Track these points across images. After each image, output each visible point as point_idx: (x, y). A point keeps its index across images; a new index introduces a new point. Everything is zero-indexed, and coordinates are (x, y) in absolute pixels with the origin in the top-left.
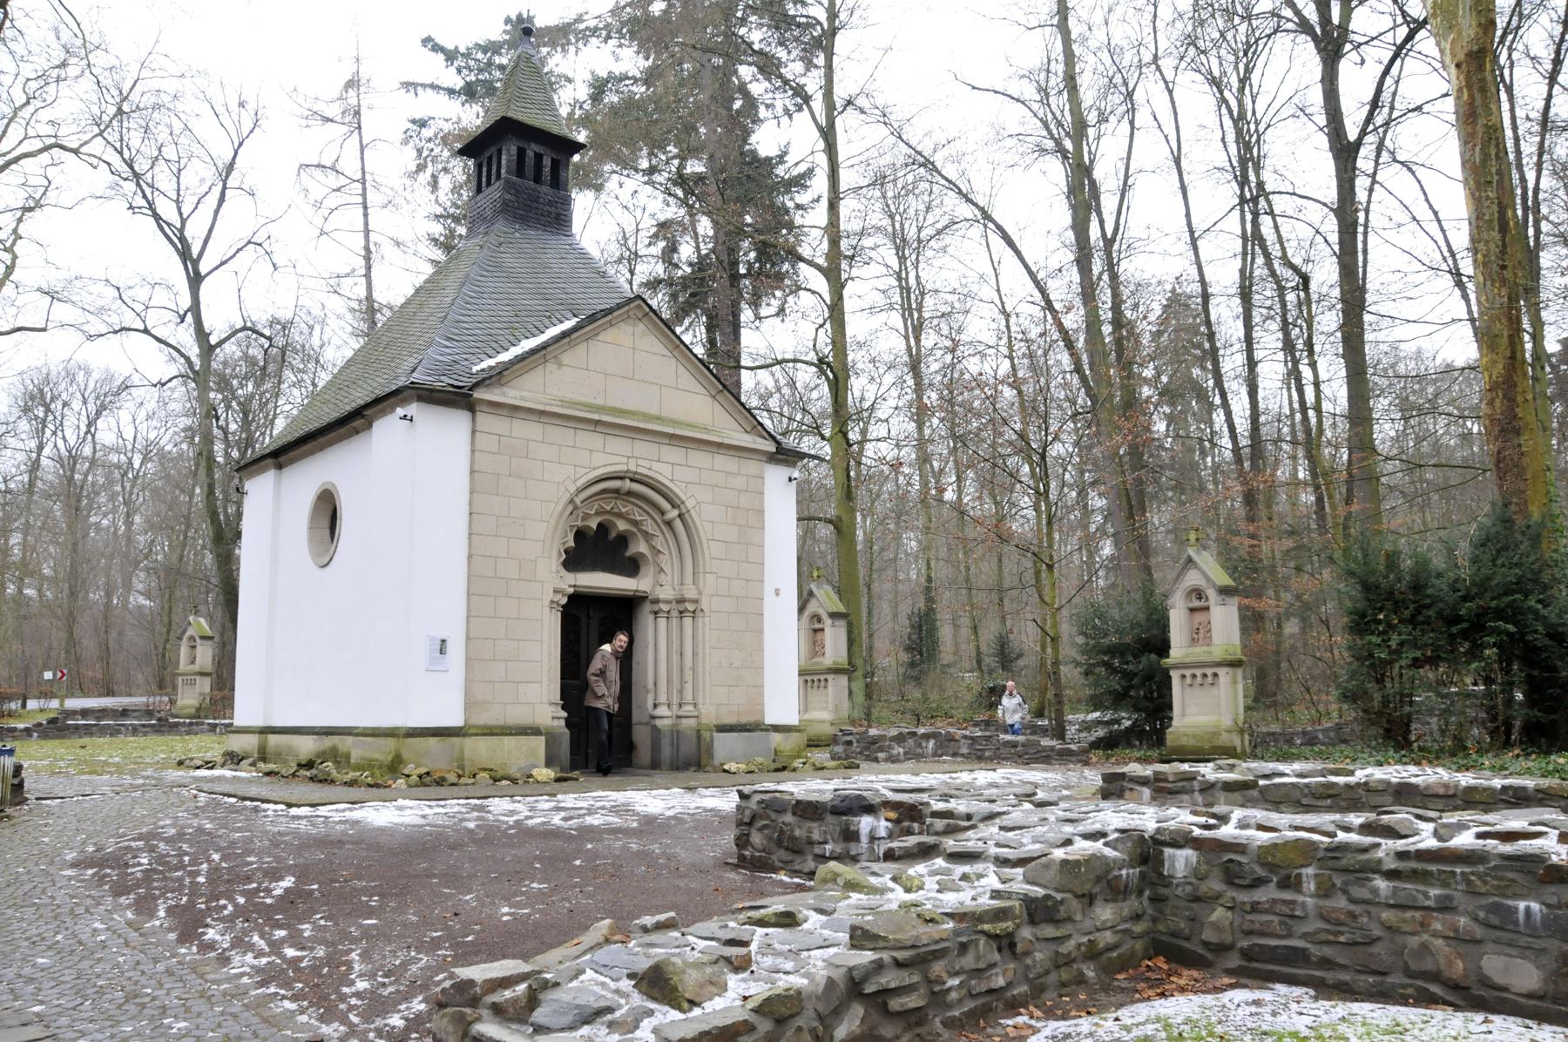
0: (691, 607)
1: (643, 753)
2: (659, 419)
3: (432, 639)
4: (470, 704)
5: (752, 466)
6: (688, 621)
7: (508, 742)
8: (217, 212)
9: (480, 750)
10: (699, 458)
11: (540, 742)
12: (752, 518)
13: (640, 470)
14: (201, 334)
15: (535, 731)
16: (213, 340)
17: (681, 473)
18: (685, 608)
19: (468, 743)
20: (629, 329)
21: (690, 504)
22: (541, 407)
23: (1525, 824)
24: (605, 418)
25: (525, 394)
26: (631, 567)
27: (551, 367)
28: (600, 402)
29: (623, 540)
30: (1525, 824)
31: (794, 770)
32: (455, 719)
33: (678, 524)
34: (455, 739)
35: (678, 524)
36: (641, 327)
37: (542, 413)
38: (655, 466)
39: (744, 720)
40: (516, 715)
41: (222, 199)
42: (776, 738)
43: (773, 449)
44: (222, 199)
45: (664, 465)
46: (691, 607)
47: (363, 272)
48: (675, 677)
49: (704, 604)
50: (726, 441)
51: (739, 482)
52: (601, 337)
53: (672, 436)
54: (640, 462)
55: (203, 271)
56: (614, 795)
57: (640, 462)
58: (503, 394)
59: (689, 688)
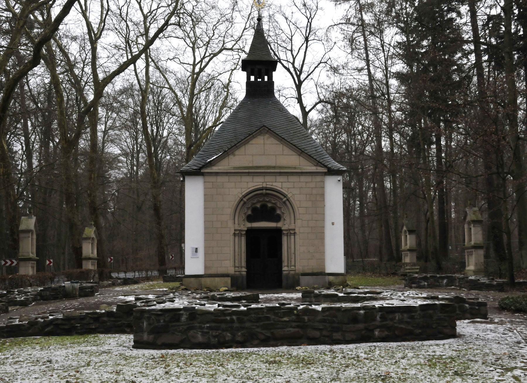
0: (292, 232)
1: (284, 283)
2: (274, 167)
3: (193, 248)
4: (206, 267)
5: (318, 178)
6: (292, 237)
7: (217, 279)
8: (305, 53)
9: (208, 281)
10: (293, 179)
11: (229, 280)
12: (319, 199)
13: (268, 186)
14: (303, 108)
15: (227, 275)
16: (307, 110)
17: (285, 185)
18: (292, 233)
19: (203, 280)
20: (262, 137)
21: (289, 196)
22: (226, 171)
23: (207, 305)
24: (251, 171)
25: (220, 168)
26: (278, 218)
27: (231, 156)
28: (251, 165)
29: (273, 209)
30: (207, 305)
31: (206, 288)
32: (201, 272)
33: (287, 202)
34: (200, 278)
35: (287, 202)
36: (267, 136)
37: (227, 173)
38: (274, 184)
39: (315, 271)
40: (221, 271)
41: (307, 47)
42: (331, 278)
43: (326, 171)
44: (307, 47)
45: (278, 184)
46: (292, 232)
47: (366, 67)
48: (295, 257)
49: (297, 231)
50: (303, 171)
51: (313, 185)
52: (250, 143)
53: (280, 173)
54: (268, 183)
55: (302, 80)
56: (276, 295)
57: (268, 183)
58: (212, 169)
59: (293, 260)
